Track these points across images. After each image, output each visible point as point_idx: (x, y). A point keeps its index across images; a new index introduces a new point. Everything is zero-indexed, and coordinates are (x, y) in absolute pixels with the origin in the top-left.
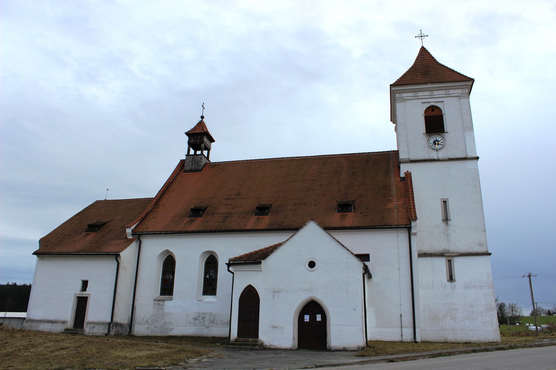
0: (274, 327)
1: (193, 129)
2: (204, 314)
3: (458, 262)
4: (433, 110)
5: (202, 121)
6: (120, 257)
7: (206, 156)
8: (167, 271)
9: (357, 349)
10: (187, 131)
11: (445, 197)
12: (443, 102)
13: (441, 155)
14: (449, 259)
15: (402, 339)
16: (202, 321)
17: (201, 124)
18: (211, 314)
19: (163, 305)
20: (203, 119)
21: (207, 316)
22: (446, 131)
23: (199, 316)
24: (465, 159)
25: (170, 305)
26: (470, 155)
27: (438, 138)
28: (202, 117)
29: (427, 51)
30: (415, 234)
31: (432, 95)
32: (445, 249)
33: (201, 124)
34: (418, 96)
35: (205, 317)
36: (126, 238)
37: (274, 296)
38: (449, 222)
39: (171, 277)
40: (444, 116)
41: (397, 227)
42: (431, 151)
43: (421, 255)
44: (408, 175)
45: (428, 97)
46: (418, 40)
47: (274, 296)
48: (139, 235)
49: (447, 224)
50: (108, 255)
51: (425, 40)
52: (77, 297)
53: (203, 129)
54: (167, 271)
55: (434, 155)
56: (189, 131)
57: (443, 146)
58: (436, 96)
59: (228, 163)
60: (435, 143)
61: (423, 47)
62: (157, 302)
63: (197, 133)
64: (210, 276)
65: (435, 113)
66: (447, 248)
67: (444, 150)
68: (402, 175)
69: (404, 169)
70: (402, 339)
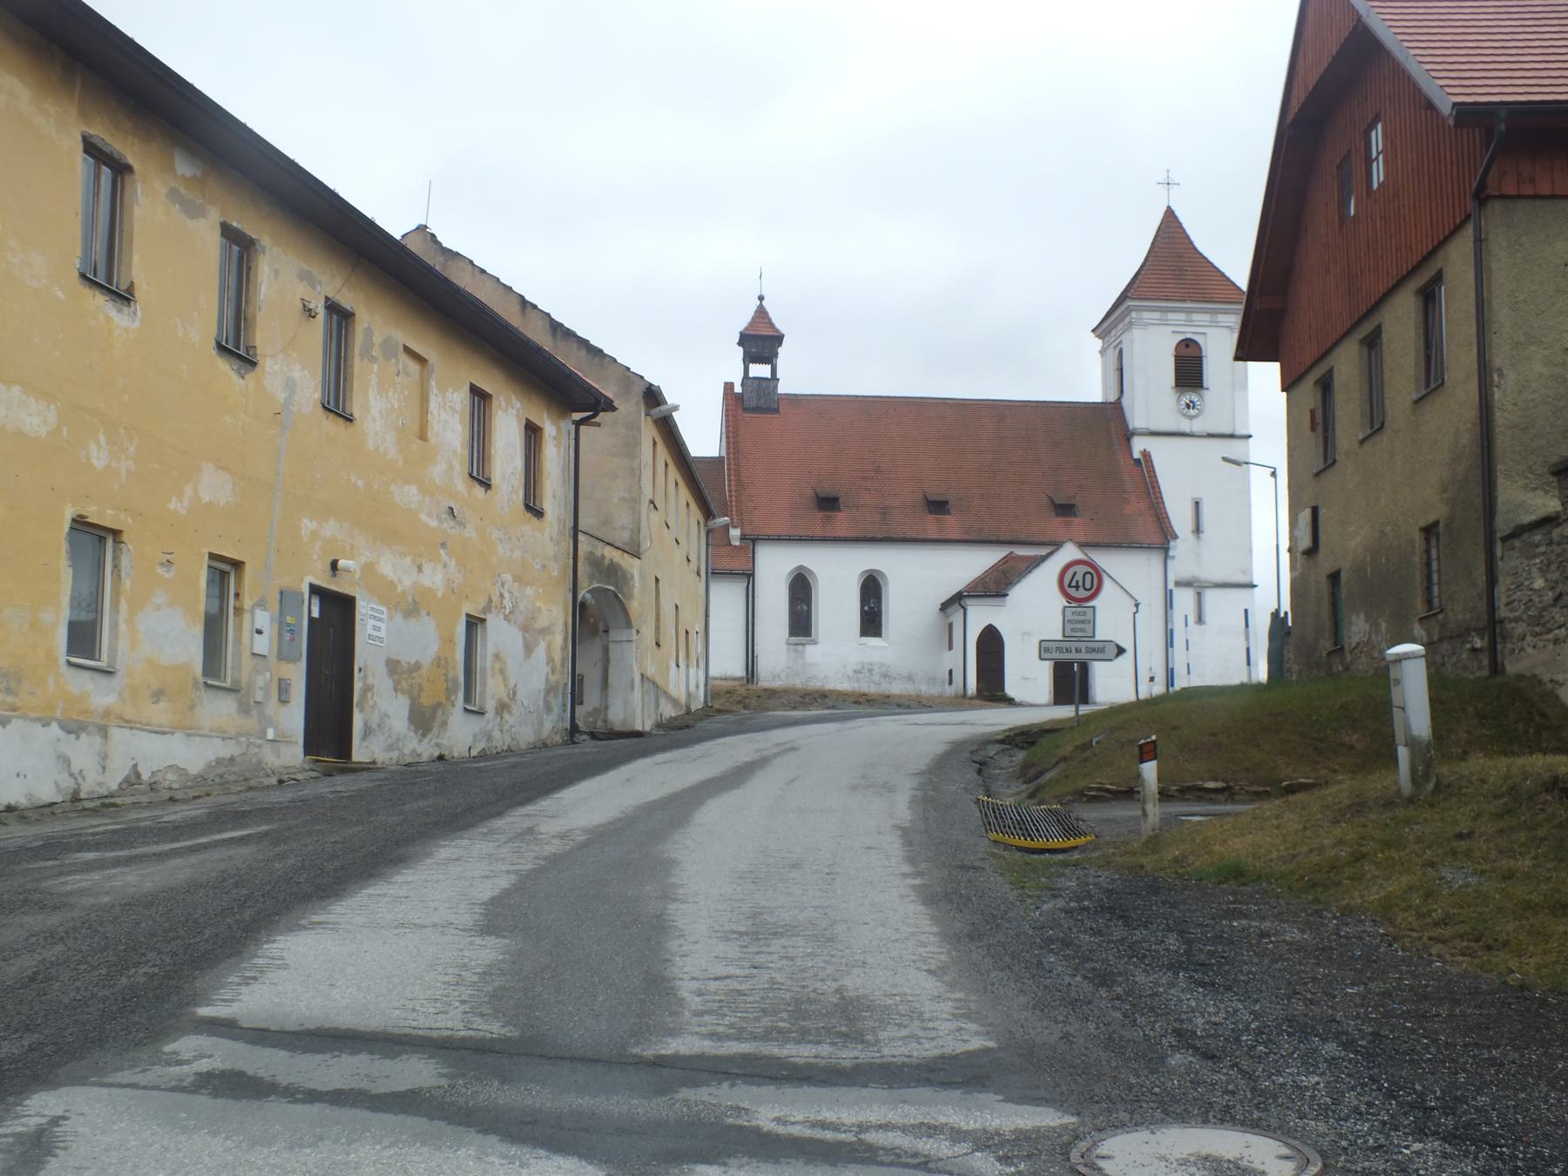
0: (1025, 679)
2: (871, 664)
3: (1210, 596)
4: (1187, 346)
5: (761, 306)
8: (798, 599)
11: (1197, 495)
12: (1205, 334)
13: (1197, 426)
14: (1199, 590)
15: (1421, 657)
16: (867, 674)
18: (882, 665)
19: (804, 651)
21: (876, 668)
22: (1205, 385)
23: (863, 668)
24: (1232, 436)
25: (813, 653)
26: (1240, 431)
27: (1195, 398)
28: (761, 298)
29: (1176, 217)
30: (1173, 558)
32: (1194, 577)
34: (1168, 320)
35: (873, 670)
36: (730, 545)
37: (1023, 639)
38: (1201, 535)
39: (805, 608)
40: (1204, 359)
41: (1150, 547)
42: (1183, 419)
43: (1178, 584)
44: (1146, 455)
46: (1162, 190)
47: (1023, 639)
48: (754, 541)
49: (1198, 538)
51: (1174, 190)
54: (798, 599)
55: (1185, 426)
57: (1201, 412)
58: (1196, 323)
60: (1188, 406)
61: (1169, 207)
62: (792, 647)
64: (870, 607)
65: (1190, 352)
66: (1197, 574)
67: (1200, 418)
68: (1136, 455)
69: (1138, 445)
70: (1421, 657)
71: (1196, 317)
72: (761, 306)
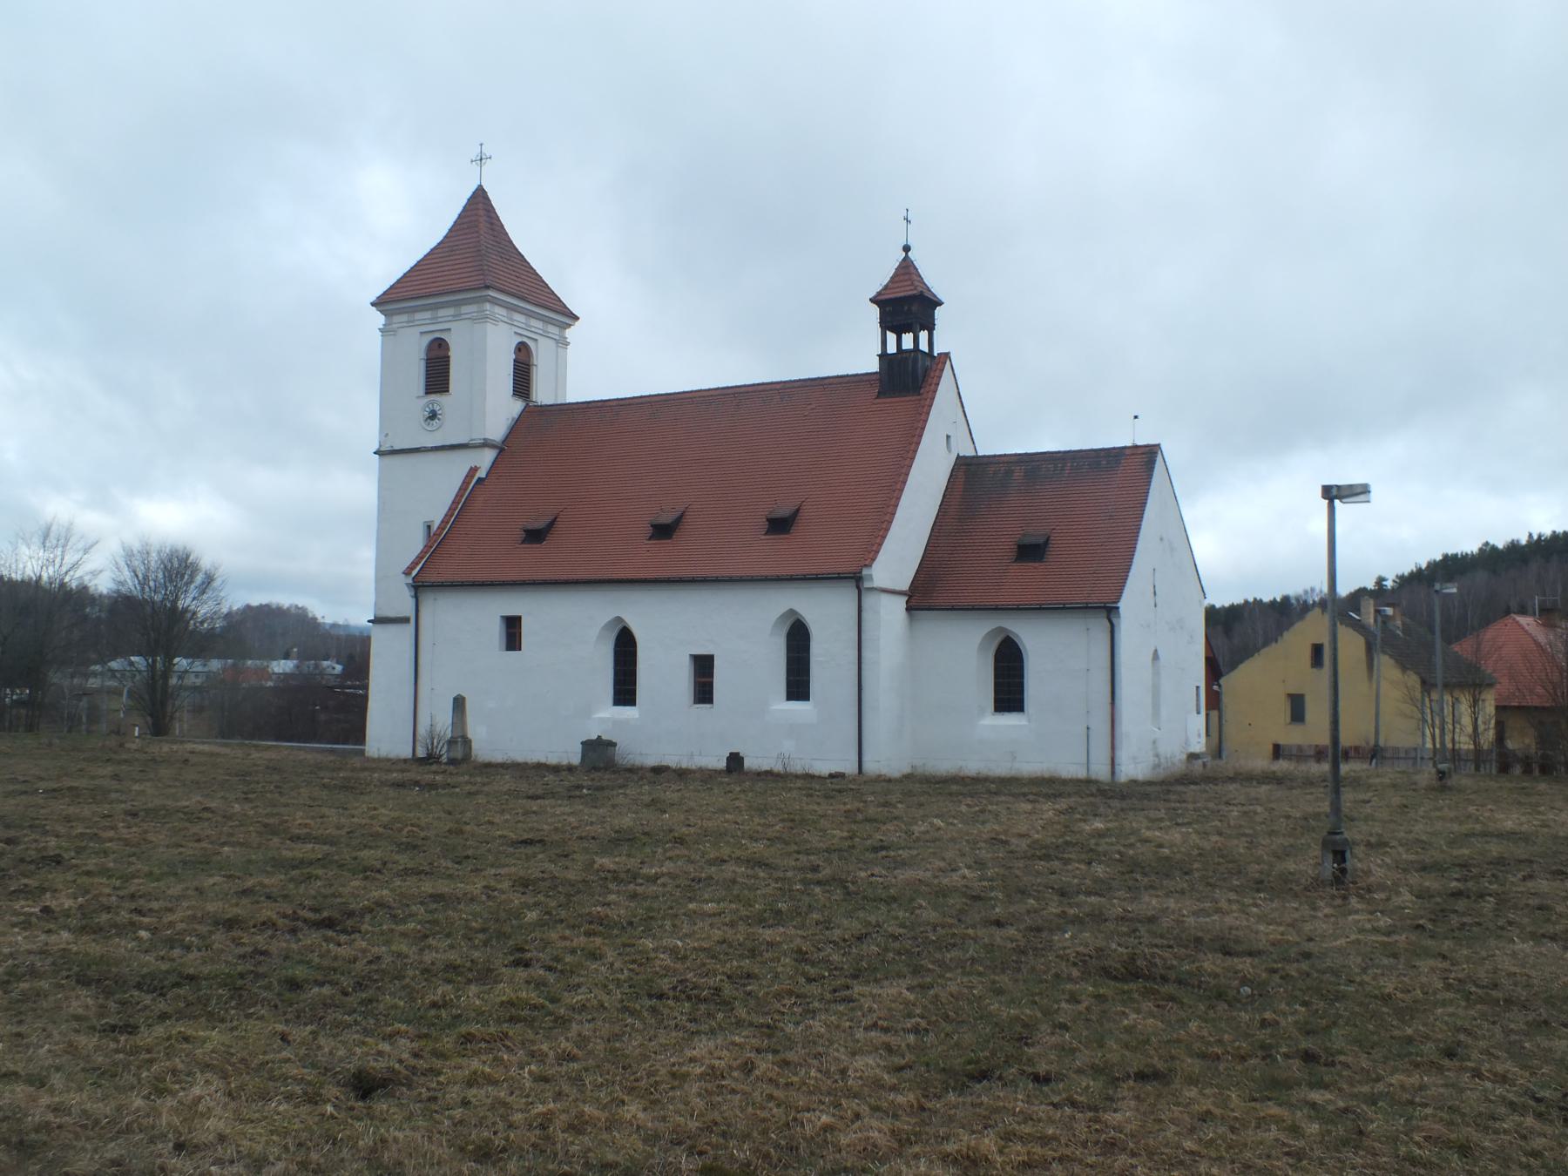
1: (886, 287)
5: (906, 259)
6: (1119, 617)
7: (927, 351)
9: (127, 575)
10: (872, 294)
15: (1113, 773)
17: (907, 269)
20: (909, 253)
28: (907, 249)
31: (412, 322)
33: (907, 269)
45: (428, 322)
50: (1086, 609)
52: (502, 617)
53: (912, 284)
56: (879, 294)
59: (769, 387)
63: (900, 298)
70: (1113, 773)
71: (442, 313)
72: (906, 259)
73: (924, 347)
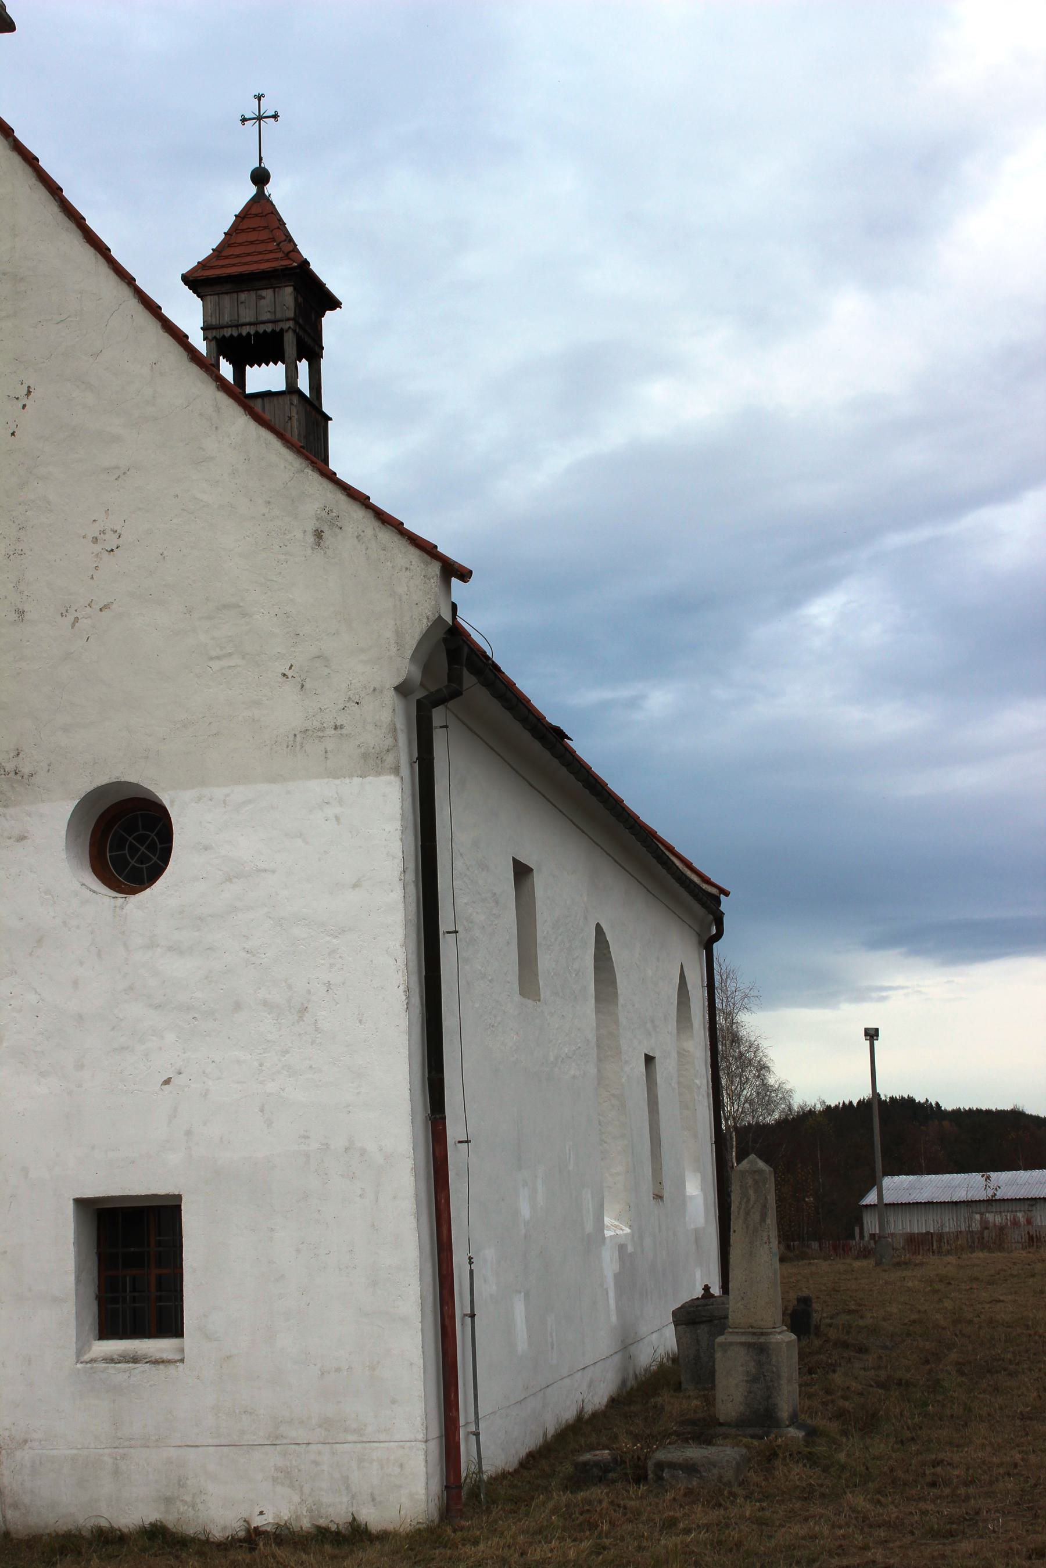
1: (218, 252)
10: (186, 269)
20: (269, 189)
28: (260, 177)
52: (81, 1204)
56: (202, 265)
73: (304, 384)
